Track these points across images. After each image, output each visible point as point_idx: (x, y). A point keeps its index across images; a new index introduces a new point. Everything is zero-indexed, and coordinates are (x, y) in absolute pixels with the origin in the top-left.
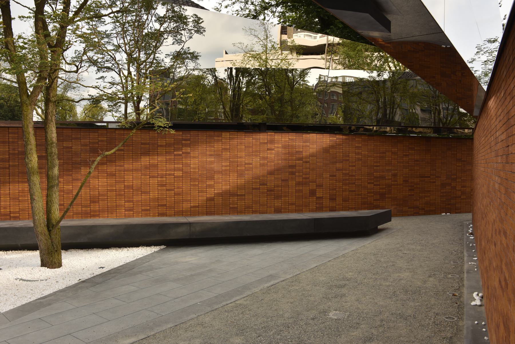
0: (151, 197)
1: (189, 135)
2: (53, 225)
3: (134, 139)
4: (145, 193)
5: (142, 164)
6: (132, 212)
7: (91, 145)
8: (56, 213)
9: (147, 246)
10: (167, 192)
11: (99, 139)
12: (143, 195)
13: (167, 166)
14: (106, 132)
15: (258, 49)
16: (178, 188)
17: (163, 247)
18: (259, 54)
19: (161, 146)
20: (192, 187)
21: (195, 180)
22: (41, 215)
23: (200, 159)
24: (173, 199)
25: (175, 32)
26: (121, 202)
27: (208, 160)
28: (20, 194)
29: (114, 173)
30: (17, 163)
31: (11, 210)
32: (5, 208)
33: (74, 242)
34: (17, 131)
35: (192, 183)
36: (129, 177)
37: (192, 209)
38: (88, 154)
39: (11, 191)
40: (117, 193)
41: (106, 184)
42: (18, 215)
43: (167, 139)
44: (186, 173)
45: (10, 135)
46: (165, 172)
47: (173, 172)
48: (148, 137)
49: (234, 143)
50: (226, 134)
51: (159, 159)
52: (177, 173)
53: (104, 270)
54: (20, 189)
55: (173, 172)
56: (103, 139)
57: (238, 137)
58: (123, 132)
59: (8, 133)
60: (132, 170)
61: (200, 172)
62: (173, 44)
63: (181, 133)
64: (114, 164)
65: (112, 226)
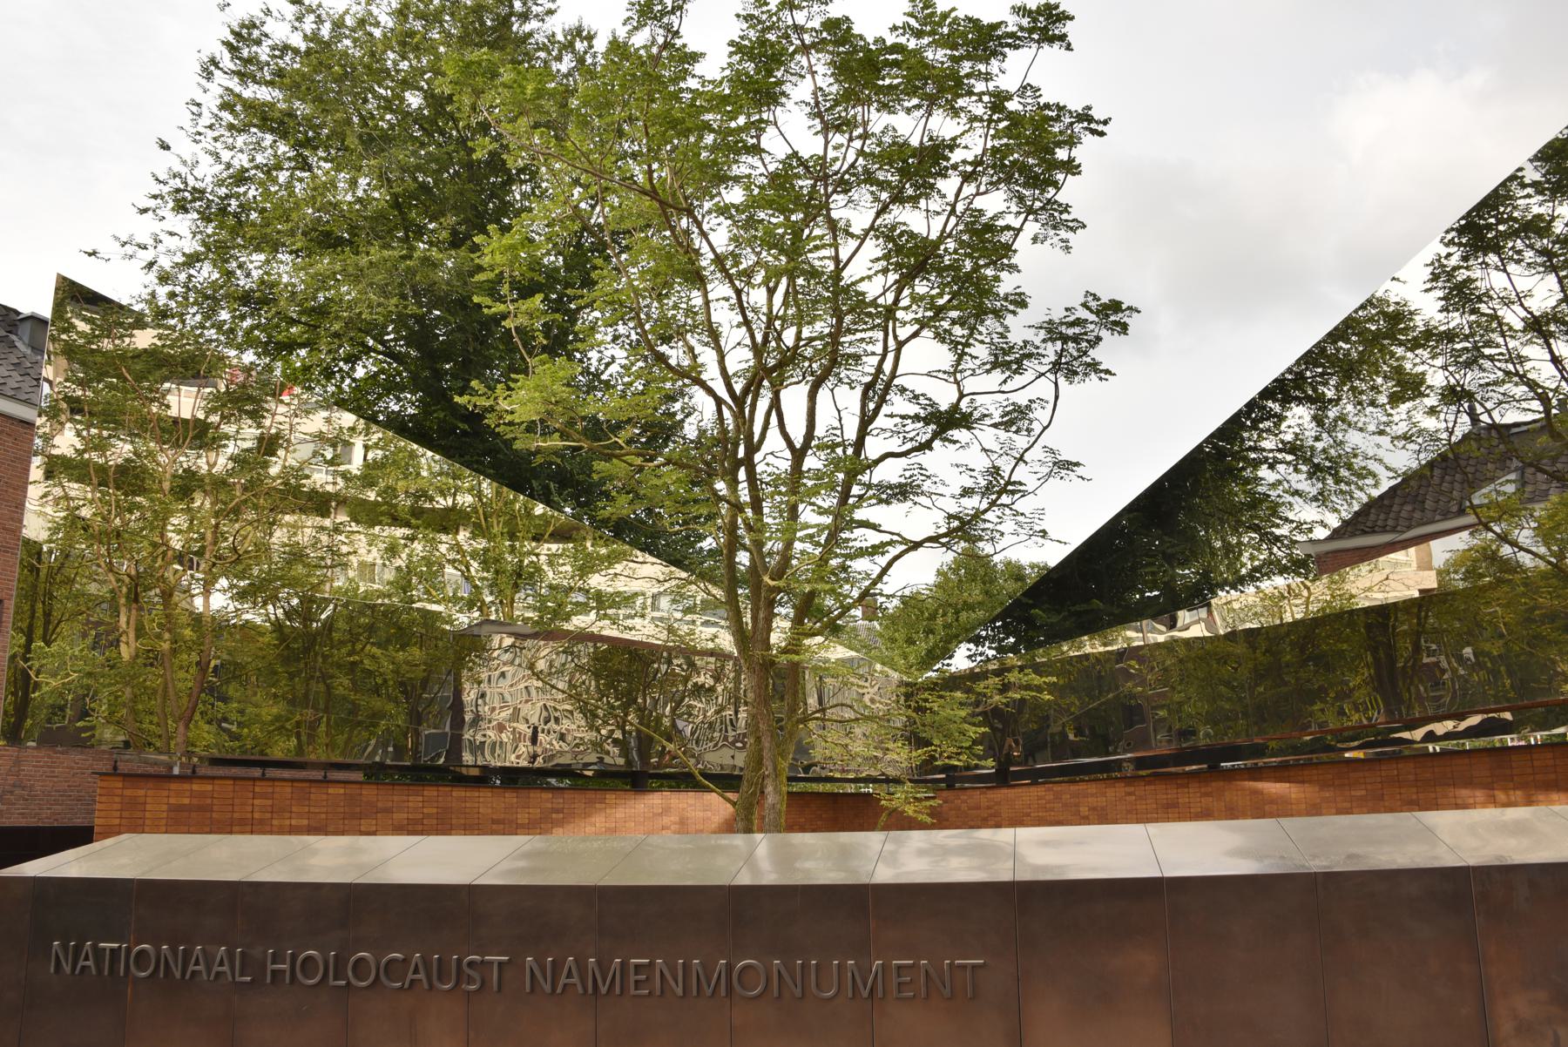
45: (257, 802)
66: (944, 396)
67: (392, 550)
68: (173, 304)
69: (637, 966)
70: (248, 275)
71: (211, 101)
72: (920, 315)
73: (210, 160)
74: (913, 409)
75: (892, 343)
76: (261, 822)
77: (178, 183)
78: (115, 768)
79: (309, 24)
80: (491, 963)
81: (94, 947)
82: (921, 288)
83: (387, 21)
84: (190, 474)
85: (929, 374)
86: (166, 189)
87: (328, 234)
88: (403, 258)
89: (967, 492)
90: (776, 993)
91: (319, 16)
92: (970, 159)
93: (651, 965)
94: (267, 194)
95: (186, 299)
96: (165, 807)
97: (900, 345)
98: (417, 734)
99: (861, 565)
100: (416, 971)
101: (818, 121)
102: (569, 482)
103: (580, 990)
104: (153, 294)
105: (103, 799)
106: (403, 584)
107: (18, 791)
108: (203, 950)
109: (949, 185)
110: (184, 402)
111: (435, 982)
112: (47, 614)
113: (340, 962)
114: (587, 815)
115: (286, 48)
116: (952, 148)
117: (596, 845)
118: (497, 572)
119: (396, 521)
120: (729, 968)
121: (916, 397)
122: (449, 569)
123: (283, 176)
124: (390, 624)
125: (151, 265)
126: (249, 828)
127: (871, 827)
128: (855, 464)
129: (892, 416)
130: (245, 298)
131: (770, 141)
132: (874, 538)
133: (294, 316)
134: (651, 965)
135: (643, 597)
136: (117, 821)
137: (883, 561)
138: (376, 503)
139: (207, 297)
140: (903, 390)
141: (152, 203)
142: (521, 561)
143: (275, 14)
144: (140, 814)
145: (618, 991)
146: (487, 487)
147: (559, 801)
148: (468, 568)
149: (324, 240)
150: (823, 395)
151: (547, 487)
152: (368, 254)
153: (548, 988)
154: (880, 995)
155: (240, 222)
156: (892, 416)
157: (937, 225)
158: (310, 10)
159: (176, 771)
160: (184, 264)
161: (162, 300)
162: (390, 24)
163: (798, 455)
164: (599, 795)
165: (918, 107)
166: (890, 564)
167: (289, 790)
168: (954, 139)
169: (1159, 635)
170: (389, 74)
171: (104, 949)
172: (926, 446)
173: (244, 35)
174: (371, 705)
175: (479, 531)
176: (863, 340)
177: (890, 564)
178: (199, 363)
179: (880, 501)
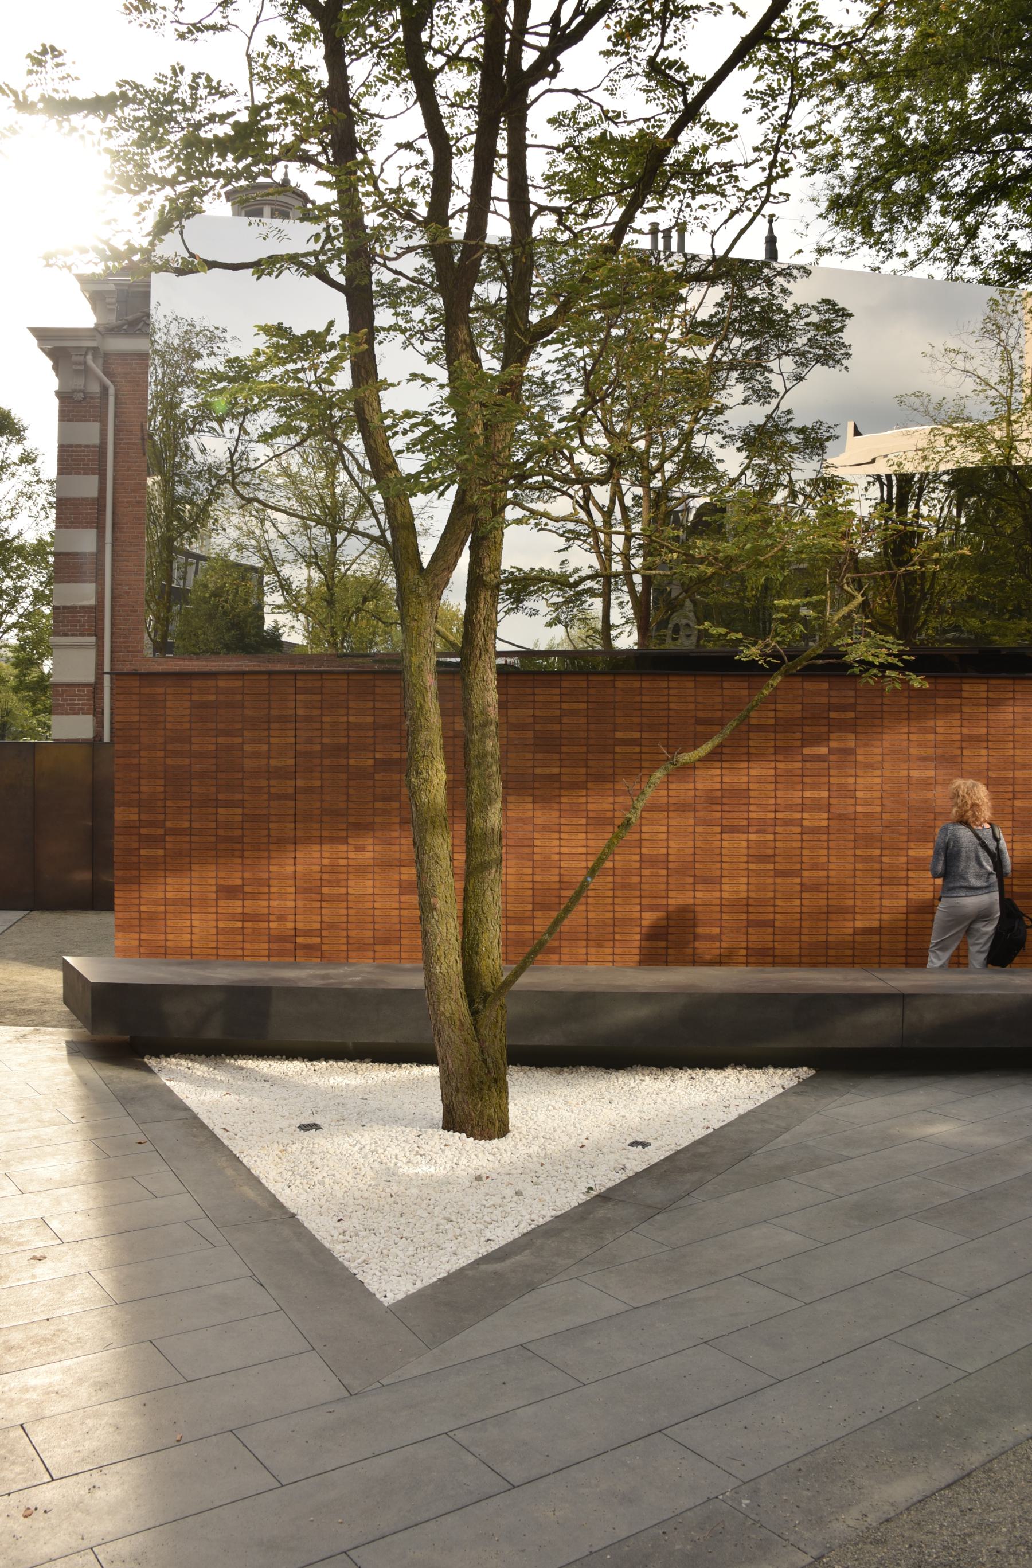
0: (725, 895)
1: (852, 693)
2: (487, 995)
3: (672, 706)
4: (707, 881)
5: (699, 786)
6: (663, 944)
7: (538, 727)
8: (493, 959)
9: (749, 1067)
10: (779, 880)
11: (565, 706)
12: (699, 887)
13: (779, 794)
14: (584, 684)
15: (980, 410)
16: (814, 867)
17: (805, 1072)
18: (982, 426)
19: (760, 728)
20: (859, 866)
21: (869, 841)
22: (453, 963)
23: (887, 773)
24: (797, 902)
25: (750, 367)
26: (627, 908)
27: (914, 773)
28: (325, 876)
29: (609, 814)
30: (318, 783)
31: (299, 926)
32: (281, 918)
33: (521, 1043)
34: (318, 684)
35: (859, 852)
36: (656, 828)
37: (858, 938)
38: (530, 756)
39: (299, 868)
40: (618, 879)
41: (583, 850)
42: (318, 940)
43: (779, 707)
44: (841, 817)
45: (299, 697)
46: (771, 815)
47: (798, 816)
48: (719, 699)
49: (1001, 717)
50: (976, 687)
51: (753, 772)
52: (810, 819)
53: (655, 1155)
54: (326, 862)
55: (798, 816)
56: (575, 706)
57: (1018, 695)
58: (637, 684)
59: (292, 690)
60: (667, 808)
61: (886, 816)
62: (746, 402)
63: (826, 686)
64: (611, 785)
65: (646, 997)
136: (136, 718)
167: (345, 683)
169: (507, 45)
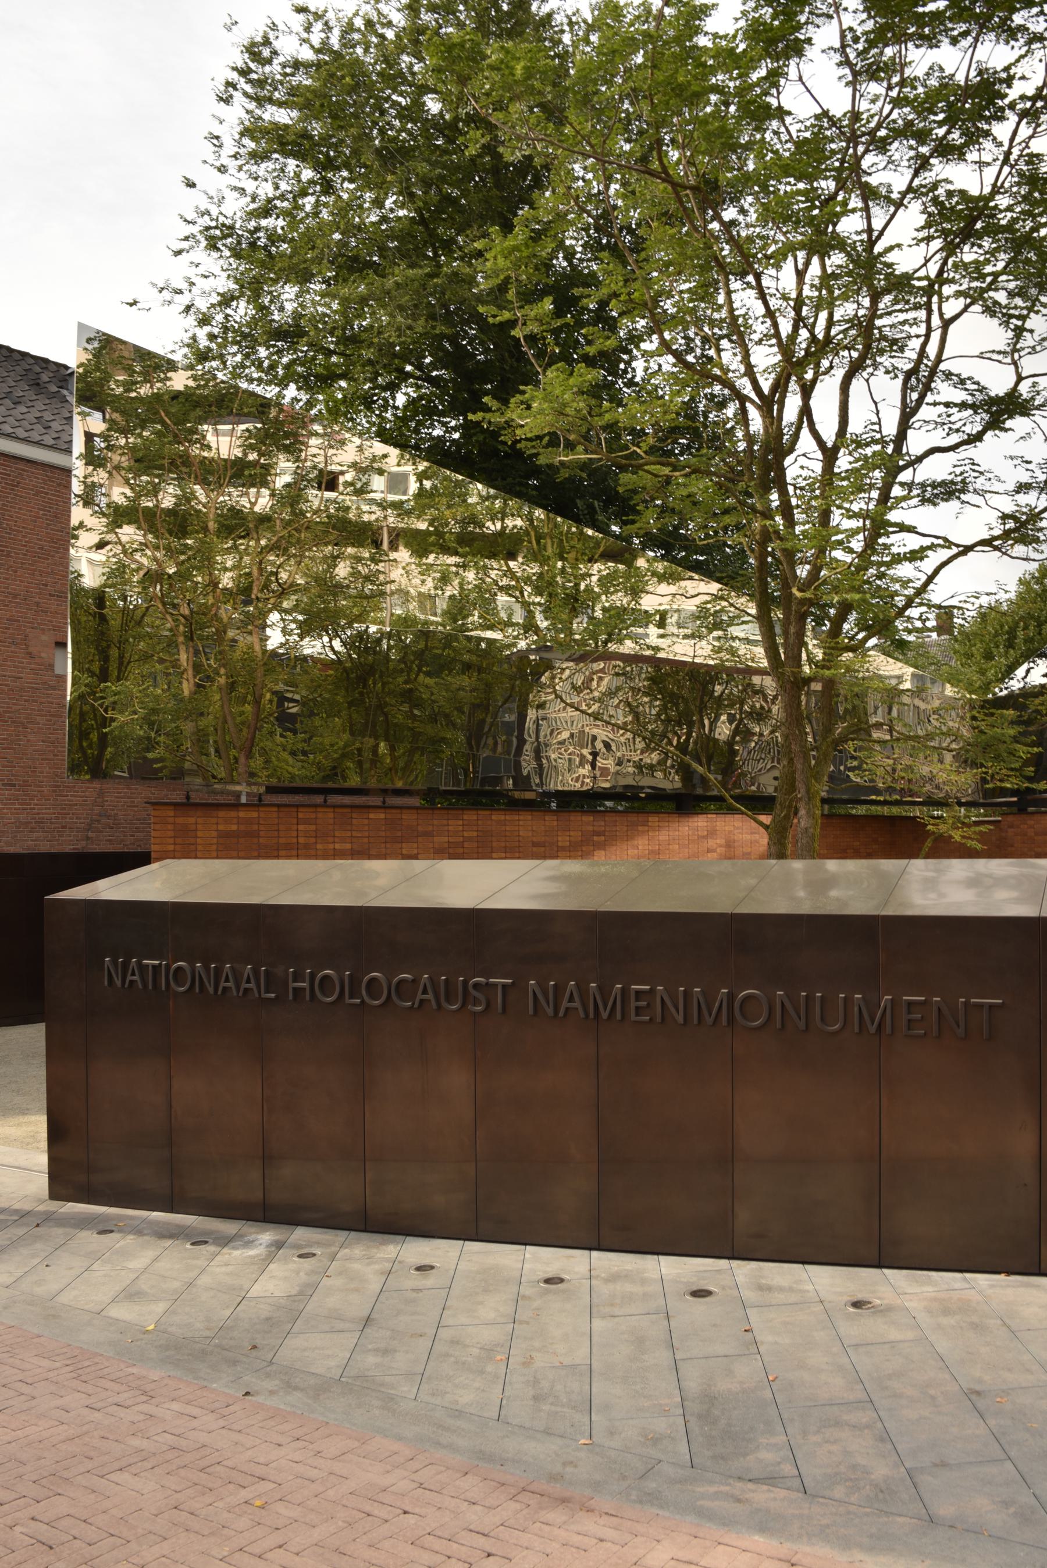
45: (301, 827)
66: (998, 381)
67: (445, 579)
68: (214, 346)
69: (638, 993)
70: (282, 309)
71: (229, 133)
72: (965, 286)
73: (236, 194)
74: (959, 396)
75: (936, 321)
76: (306, 846)
77: (206, 221)
78: (188, 797)
79: (316, 37)
80: (495, 985)
81: (139, 963)
82: (969, 254)
83: (399, 19)
84: (235, 513)
85: (981, 356)
86: (195, 229)
87: (355, 259)
88: (431, 276)
89: (1022, 488)
90: (779, 1025)
91: (326, 24)
92: (1030, 92)
93: (652, 991)
94: (293, 224)
95: (225, 339)
96: (214, 834)
97: (946, 324)
98: (475, 758)
99: (905, 570)
100: (425, 992)
101: (847, 71)
102: (589, 498)
103: (582, 1015)
104: (194, 338)
105: (157, 827)
106: (458, 609)
107: (104, 820)
108: (232, 968)
109: (1002, 130)
110: (223, 441)
111: (444, 1004)
112: (121, 657)
113: (355, 981)
114: (629, 838)
115: (297, 65)
116: (1009, 81)
117: (603, 869)
118: (550, 595)
119: (446, 550)
120: (731, 997)
121: (962, 382)
122: (502, 599)
123: (308, 202)
124: (435, 652)
125: (188, 309)
126: (294, 852)
127: (912, 854)
128: (893, 459)
129: (935, 404)
130: (280, 333)
131: (790, 96)
132: (913, 542)
133: (332, 347)
134: (652, 991)
135: (680, 616)
136: (171, 847)
137: (928, 565)
138: (426, 533)
139: (245, 336)
140: (948, 375)
141: (185, 245)
142: (577, 585)
143: (281, 27)
144: (192, 840)
145: (619, 1016)
146: (539, 513)
147: (600, 824)
148: (522, 593)
149: (351, 266)
150: (857, 385)
151: (591, 507)
152: (393, 274)
153: (550, 1011)
154: (888, 1030)
155: (270, 254)
156: (935, 404)
157: (990, 174)
158: (318, 16)
159: (244, 800)
160: (220, 304)
161: (203, 342)
162: (403, 23)
163: (830, 455)
164: (642, 818)
165: (965, 34)
166: (937, 571)
167: (331, 815)
168: (1007, 69)
170: (405, 79)
171: (147, 965)
172: (978, 438)
173: (257, 51)
174: (433, 736)
175: (535, 556)
176: (904, 322)
177: (937, 571)
178: (231, 401)
179: (924, 501)
